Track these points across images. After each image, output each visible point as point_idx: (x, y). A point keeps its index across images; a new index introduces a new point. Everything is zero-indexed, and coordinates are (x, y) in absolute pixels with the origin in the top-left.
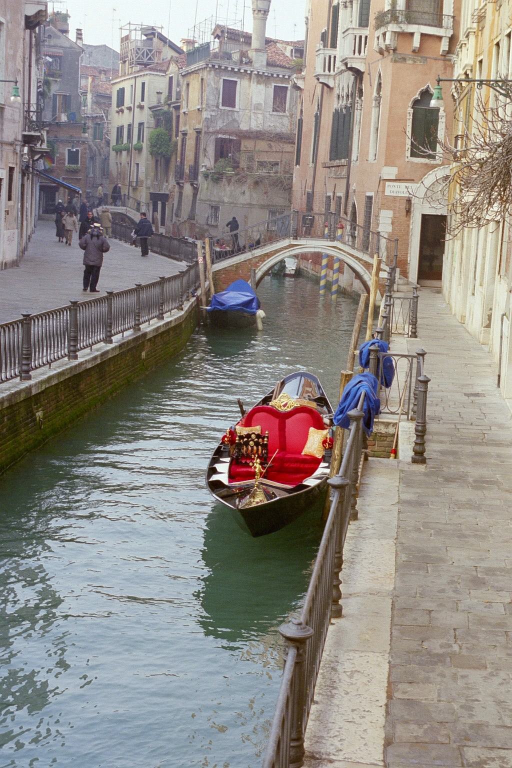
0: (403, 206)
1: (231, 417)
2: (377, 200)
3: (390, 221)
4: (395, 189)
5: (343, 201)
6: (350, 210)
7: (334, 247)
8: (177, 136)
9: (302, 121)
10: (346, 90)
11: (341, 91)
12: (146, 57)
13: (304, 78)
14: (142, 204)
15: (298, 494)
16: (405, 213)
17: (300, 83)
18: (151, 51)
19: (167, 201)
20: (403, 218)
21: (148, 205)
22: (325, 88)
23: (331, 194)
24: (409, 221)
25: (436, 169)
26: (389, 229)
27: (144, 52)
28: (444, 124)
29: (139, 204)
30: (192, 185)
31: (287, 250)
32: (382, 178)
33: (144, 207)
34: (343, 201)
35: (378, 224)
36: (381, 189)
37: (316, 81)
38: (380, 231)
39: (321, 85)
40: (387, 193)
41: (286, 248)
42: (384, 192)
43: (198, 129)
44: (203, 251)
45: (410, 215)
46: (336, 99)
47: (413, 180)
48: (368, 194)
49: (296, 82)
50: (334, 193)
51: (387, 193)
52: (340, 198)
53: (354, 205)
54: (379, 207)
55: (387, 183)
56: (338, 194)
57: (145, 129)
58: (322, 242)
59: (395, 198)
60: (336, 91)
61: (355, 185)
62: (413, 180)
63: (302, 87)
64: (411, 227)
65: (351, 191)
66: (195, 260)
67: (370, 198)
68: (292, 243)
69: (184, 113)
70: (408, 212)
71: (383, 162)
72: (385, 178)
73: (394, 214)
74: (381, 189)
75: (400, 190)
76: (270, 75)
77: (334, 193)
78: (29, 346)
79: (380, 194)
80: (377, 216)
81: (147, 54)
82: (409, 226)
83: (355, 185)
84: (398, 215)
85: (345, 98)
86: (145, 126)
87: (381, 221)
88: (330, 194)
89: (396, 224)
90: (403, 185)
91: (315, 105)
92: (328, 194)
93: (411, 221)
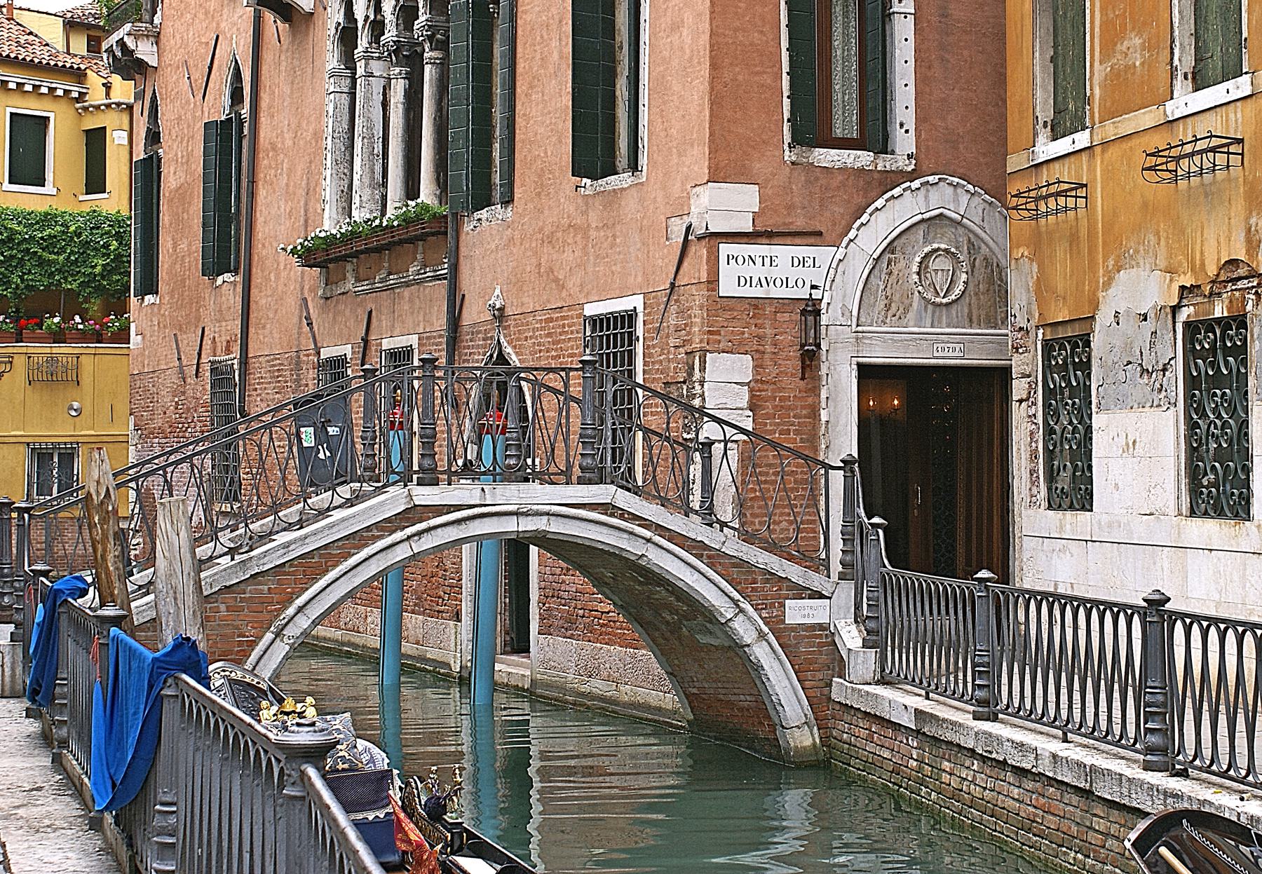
0: (789, 336)
1: (605, 788)
4: (757, 271)
13: (157, 36)
15: (610, 868)
17: (145, 51)
20: (792, 384)
24: (815, 391)
25: (897, 191)
28: (911, 18)
31: (398, 536)
40: (727, 288)
42: (713, 281)
47: (820, 234)
51: (727, 288)
55: (725, 249)
58: (400, 132)
64: (824, 418)
70: (810, 358)
75: (775, 273)
78: (1163, 685)
82: (814, 413)
84: (771, 371)
90: (784, 253)
93: (824, 395)
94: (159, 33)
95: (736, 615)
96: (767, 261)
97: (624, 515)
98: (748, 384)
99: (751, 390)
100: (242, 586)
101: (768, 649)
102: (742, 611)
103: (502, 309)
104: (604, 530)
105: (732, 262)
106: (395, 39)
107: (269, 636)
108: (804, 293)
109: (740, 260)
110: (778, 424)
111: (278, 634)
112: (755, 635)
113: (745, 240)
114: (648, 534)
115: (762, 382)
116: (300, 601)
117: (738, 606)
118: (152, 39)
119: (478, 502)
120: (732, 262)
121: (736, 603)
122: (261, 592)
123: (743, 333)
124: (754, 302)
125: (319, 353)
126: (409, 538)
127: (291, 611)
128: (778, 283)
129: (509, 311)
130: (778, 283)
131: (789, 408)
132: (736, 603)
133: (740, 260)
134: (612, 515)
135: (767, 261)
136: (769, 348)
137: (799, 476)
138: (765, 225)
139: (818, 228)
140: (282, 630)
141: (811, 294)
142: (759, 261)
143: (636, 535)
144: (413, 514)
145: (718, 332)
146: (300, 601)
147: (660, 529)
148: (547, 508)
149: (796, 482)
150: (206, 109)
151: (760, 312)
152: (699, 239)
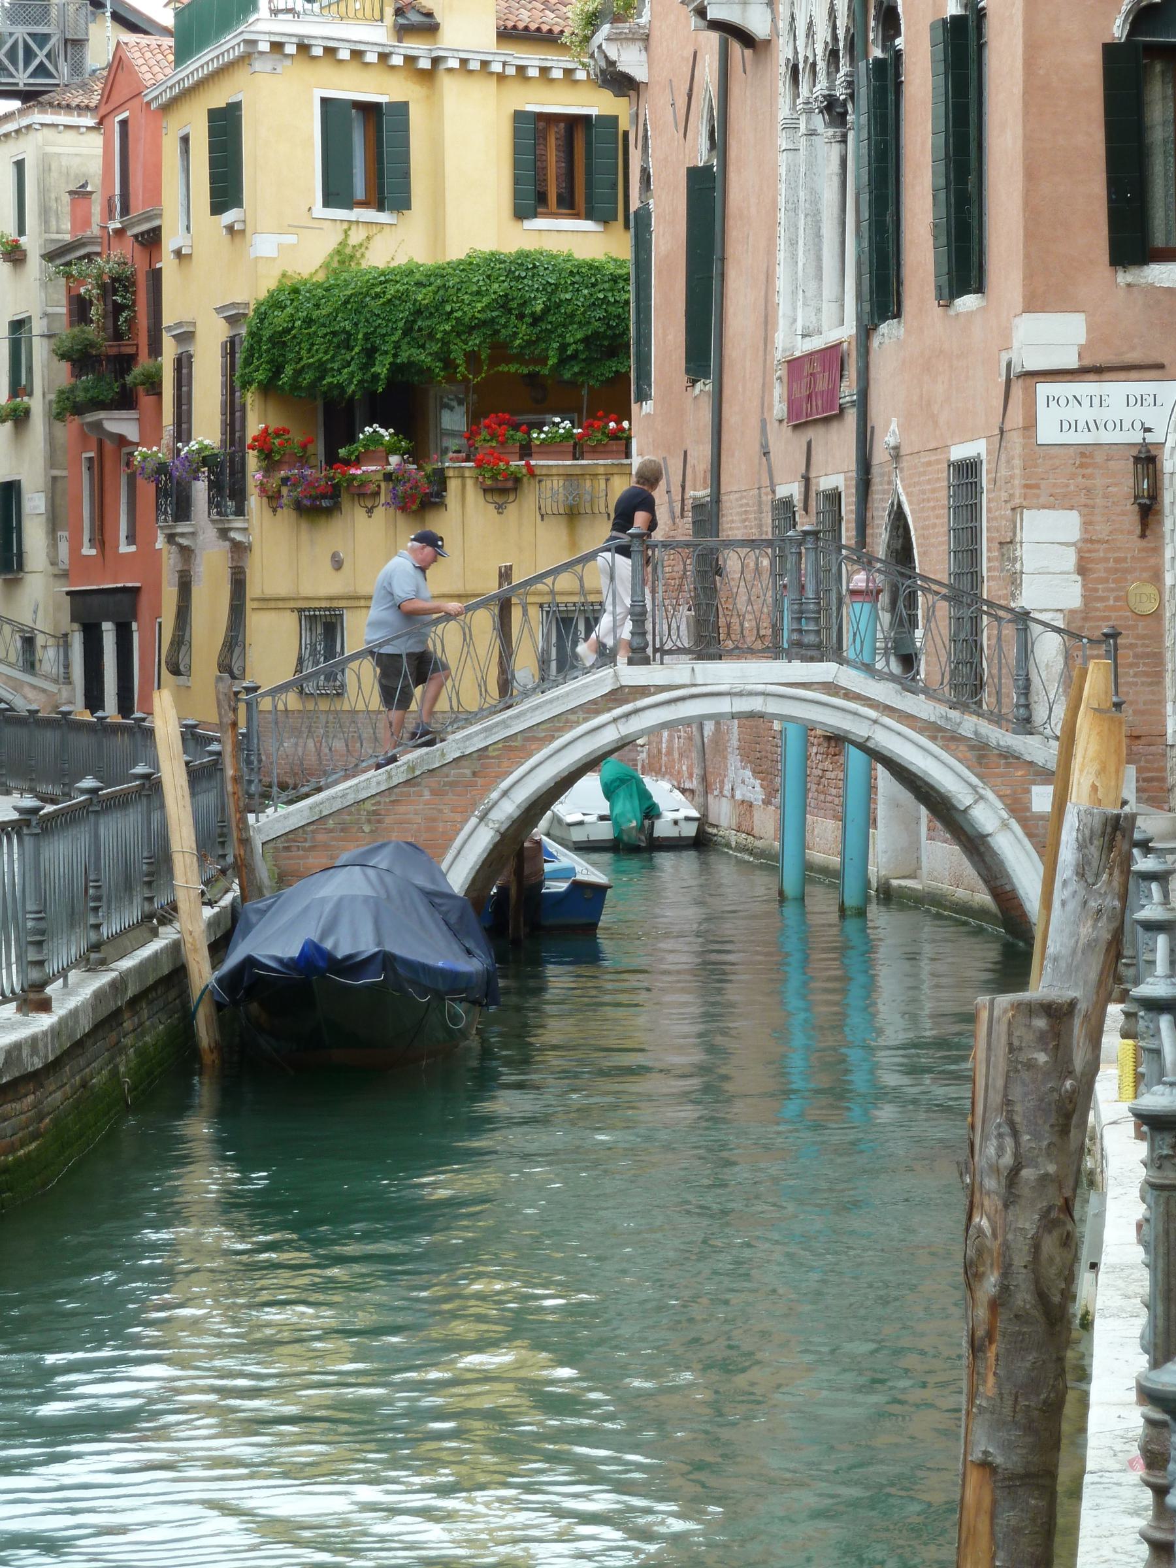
2: (1003, 472)
3: (1069, 559)
4: (1084, 414)
5: (848, 508)
6: (880, 540)
7: (831, 688)
8: (156, 349)
9: (649, 215)
10: (822, 34)
11: (801, 43)
12: (26, 65)
13: (646, 38)
14: (40, 640)
16: (1130, 518)
17: (631, 61)
18: (42, 39)
19: (136, 619)
21: (64, 641)
22: (736, 47)
23: (791, 489)
26: (1071, 595)
27: (14, 46)
29: (29, 642)
30: (224, 533)
32: (1017, 369)
33: (51, 653)
34: (848, 508)
35: (1015, 580)
36: (1016, 417)
37: (694, 21)
38: (1028, 607)
39: (714, 37)
40: (1048, 432)
41: (594, 708)
42: (1030, 426)
43: (234, 305)
44: (954, 1357)
45: (1160, 523)
46: (782, 85)
47: (1160, 366)
48: (959, 452)
49: (613, 56)
50: (807, 480)
51: (1048, 432)
52: (834, 497)
53: (898, 518)
54: (1017, 501)
55: (1044, 389)
56: (824, 483)
57: (36, 341)
59: (1085, 454)
60: (783, 52)
61: (894, 426)
62: (1160, 366)
63: (640, 74)
65: (880, 456)
66: (140, 769)
67: (967, 471)
68: (625, 681)
69: (178, 253)
71: (1019, 307)
72: (1030, 366)
73: (1087, 524)
74: (1016, 417)
76: (511, 71)
77: (807, 480)
79: (1015, 440)
80: (1007, 544)
81: (29, 54)
83: (894, 426)
85: (821, 65)
86: (36, 330)
87: (1030, 557)
88: (791, 489)
89: (1100, 570)
90: (1116, 390)
91: (698, 133)
92: (782, 491)
94: (648, 36)
95: (976, 802)
96: (1096, 401)
97: (849, 695)
98: (1074, 544)
99: (1079, 551)
100: (445, 769)
101: (1012, 838)
102: (981, 797)
103: (896, 448)
104: (828, 711)
105: (1053, 404)
106: (827, 92)
107: (473, 821)
108: (1137, 437)
109: (1063, 401)
110: (1113, 590)
111: (482, 819)
112: (997, 823)
113: (1069, 377)
114: (873, 714)
115: (1091, 541)
116: (505, 784)
117: (977, 792)
118: (640, 44)
119: (688, 682)
120: (1053, 404)
121: (974, 788)
122: (463, 775)
123: (1067, 486)
124: (1082, 449)
125: (774, 492)
126: (615, 720)
127: (495, 795)
128: (1110, 426)
129: (903, 452)
130: (1110, 426)
131: (1126, 571)
132: (974, 788)
133: (1063, 401)
134: (836, 695)
135: (1096, 401)
136: (1099, 501)
137: (1139, 650)
138: (1087, 362)
139: (1160, 360)
140: (486, 814)
141: (1144, 439)
142: (1086, 402)
143: (860, 715)
144: (618, 695)
145: (1037, 486)
146: (505, 784)
147: (888, 710)
148: (760, 688)
149: (1136, 656)
150: (687, 151)
151: (1088, 460)
152: (1018, 377)
